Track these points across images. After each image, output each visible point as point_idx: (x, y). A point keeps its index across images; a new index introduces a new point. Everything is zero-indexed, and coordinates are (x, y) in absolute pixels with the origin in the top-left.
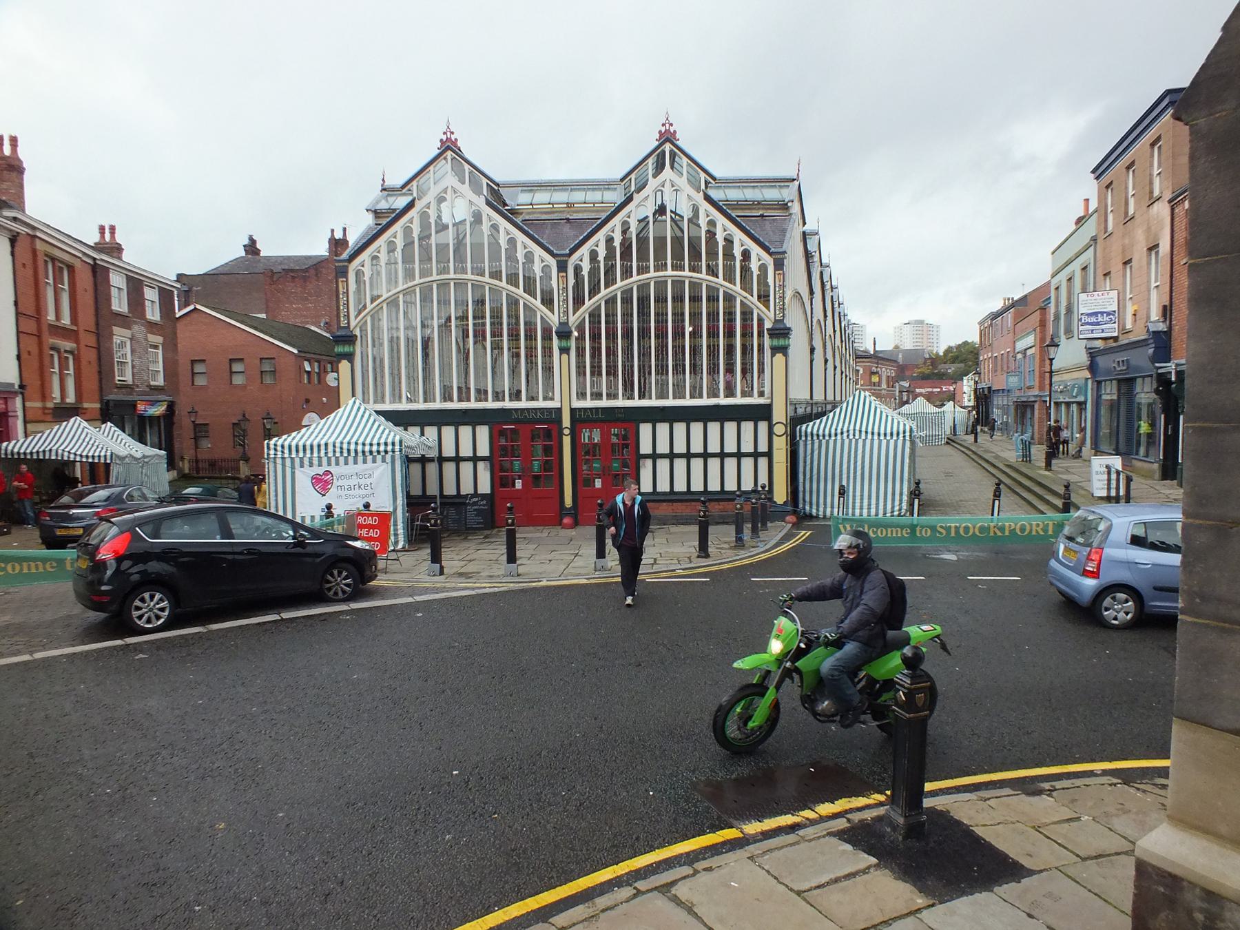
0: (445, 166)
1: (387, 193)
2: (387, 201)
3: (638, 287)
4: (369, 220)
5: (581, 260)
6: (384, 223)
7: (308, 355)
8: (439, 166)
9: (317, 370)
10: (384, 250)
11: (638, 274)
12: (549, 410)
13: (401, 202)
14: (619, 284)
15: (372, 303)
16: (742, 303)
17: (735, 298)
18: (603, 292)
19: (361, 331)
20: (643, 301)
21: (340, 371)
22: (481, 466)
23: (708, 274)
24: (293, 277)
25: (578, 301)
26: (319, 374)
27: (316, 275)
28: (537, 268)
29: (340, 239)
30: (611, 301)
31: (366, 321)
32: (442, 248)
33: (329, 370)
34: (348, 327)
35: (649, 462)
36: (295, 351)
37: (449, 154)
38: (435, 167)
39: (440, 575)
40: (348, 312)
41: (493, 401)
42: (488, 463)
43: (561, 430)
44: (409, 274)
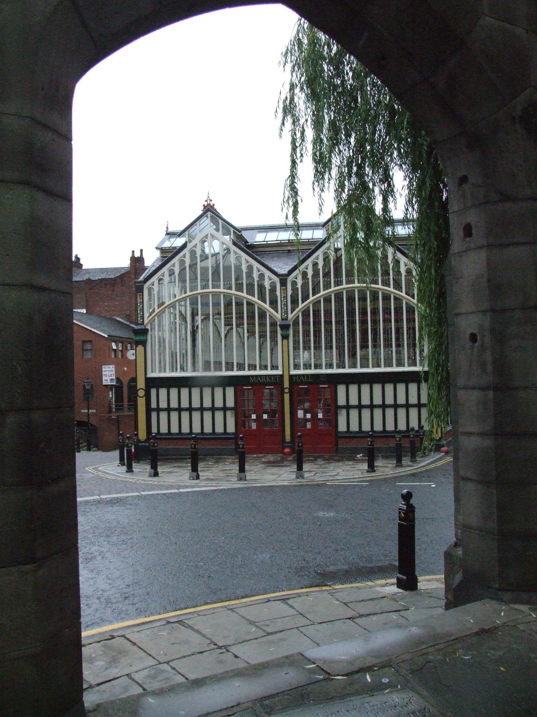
1: (169, 236)
2: (170, 241)
3: (335, 295)
4: (158, 254)
6: (169, 256)
7: (115, 338)
8: (202, 221)
9: (120, 348)
12: (274, 376)
13: (179, 242)
15: (158, 308)
17: (402, 300)
18: (311, 298)
19: (151, 326)
20: (351, 300)
21: (144, 379)
22: (229, 414)
23: (383, 285)
25: (295, 302)
26: (122, 351)
28: (267, 284)
30: (317, 303)
32: (205, 270)
33: (129, 348)
34: (143, 323)
35: (344, 412)
36: (106, 336)
37: (209, 214)
38: (200, 222)
39: (197, 479)
42: (233, 412)
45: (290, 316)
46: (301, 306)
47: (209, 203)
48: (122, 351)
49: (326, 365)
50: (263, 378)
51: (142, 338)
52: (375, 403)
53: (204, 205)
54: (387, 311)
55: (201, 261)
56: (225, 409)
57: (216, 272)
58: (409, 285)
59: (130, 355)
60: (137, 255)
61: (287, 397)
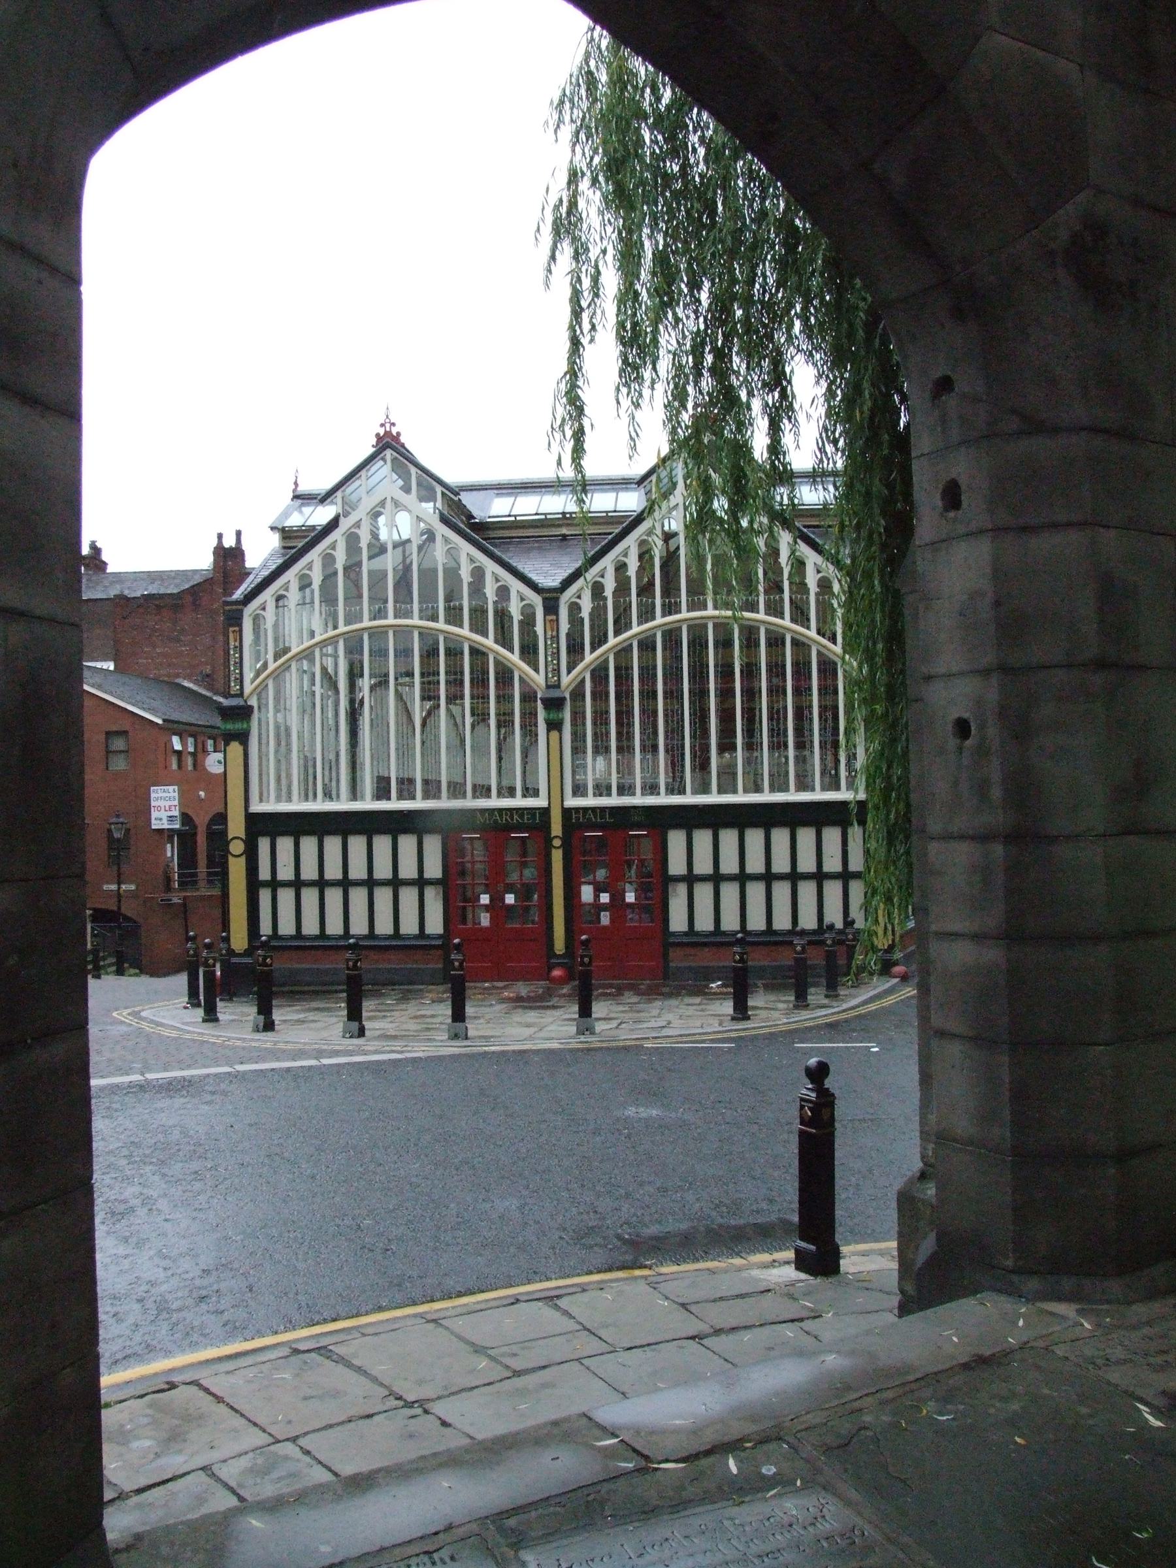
0: (382, 470)
2: (301, 512)
4: (275, 540)
5: (603, 576)
6: (300, 545)
8: (374, 469)
9: (191, 749)
10: (294, 586)
11: (664, 615)
12: (531, 811)
13: (321, 515)
14: (636, 629)
15: (275, 661)
16: (819, 653)
20: (698, 644)
22: (431, 893)
24: (158, 607)
25: (576, 649)
26: (194, 755)
27: (194, 603)
28: (515, 609)
29: (231, 549)
30: (624, 652)
31: (267, 685)
32: (378, 578)
33: (210, 748)
34: (241, 695)
35: (682, 889)
36: (160, 721)
37: (389, 453)
40: (241, 674)
41: (449, 798)
42: (440, 889)
43: (548, 840)
44: (669, 609)
45: (566, 680)
46: (589, 657)
47: (388, 429)
48: (194, 755)
49: (643, 788)
50: (506, 815)
51: (239, 726)
52: (750, 869)
53: (378, 435)
54: (776, 669)
55: (370, 558)
56: (421, 883)
57: (403, 583)
58: (825, 611)
59: (213, 763)
60: (229, 542)
61: (557, 856)
